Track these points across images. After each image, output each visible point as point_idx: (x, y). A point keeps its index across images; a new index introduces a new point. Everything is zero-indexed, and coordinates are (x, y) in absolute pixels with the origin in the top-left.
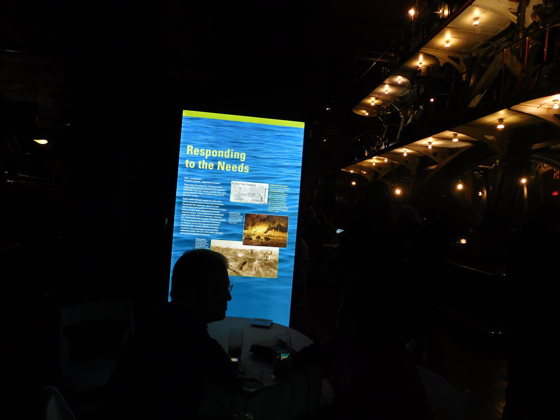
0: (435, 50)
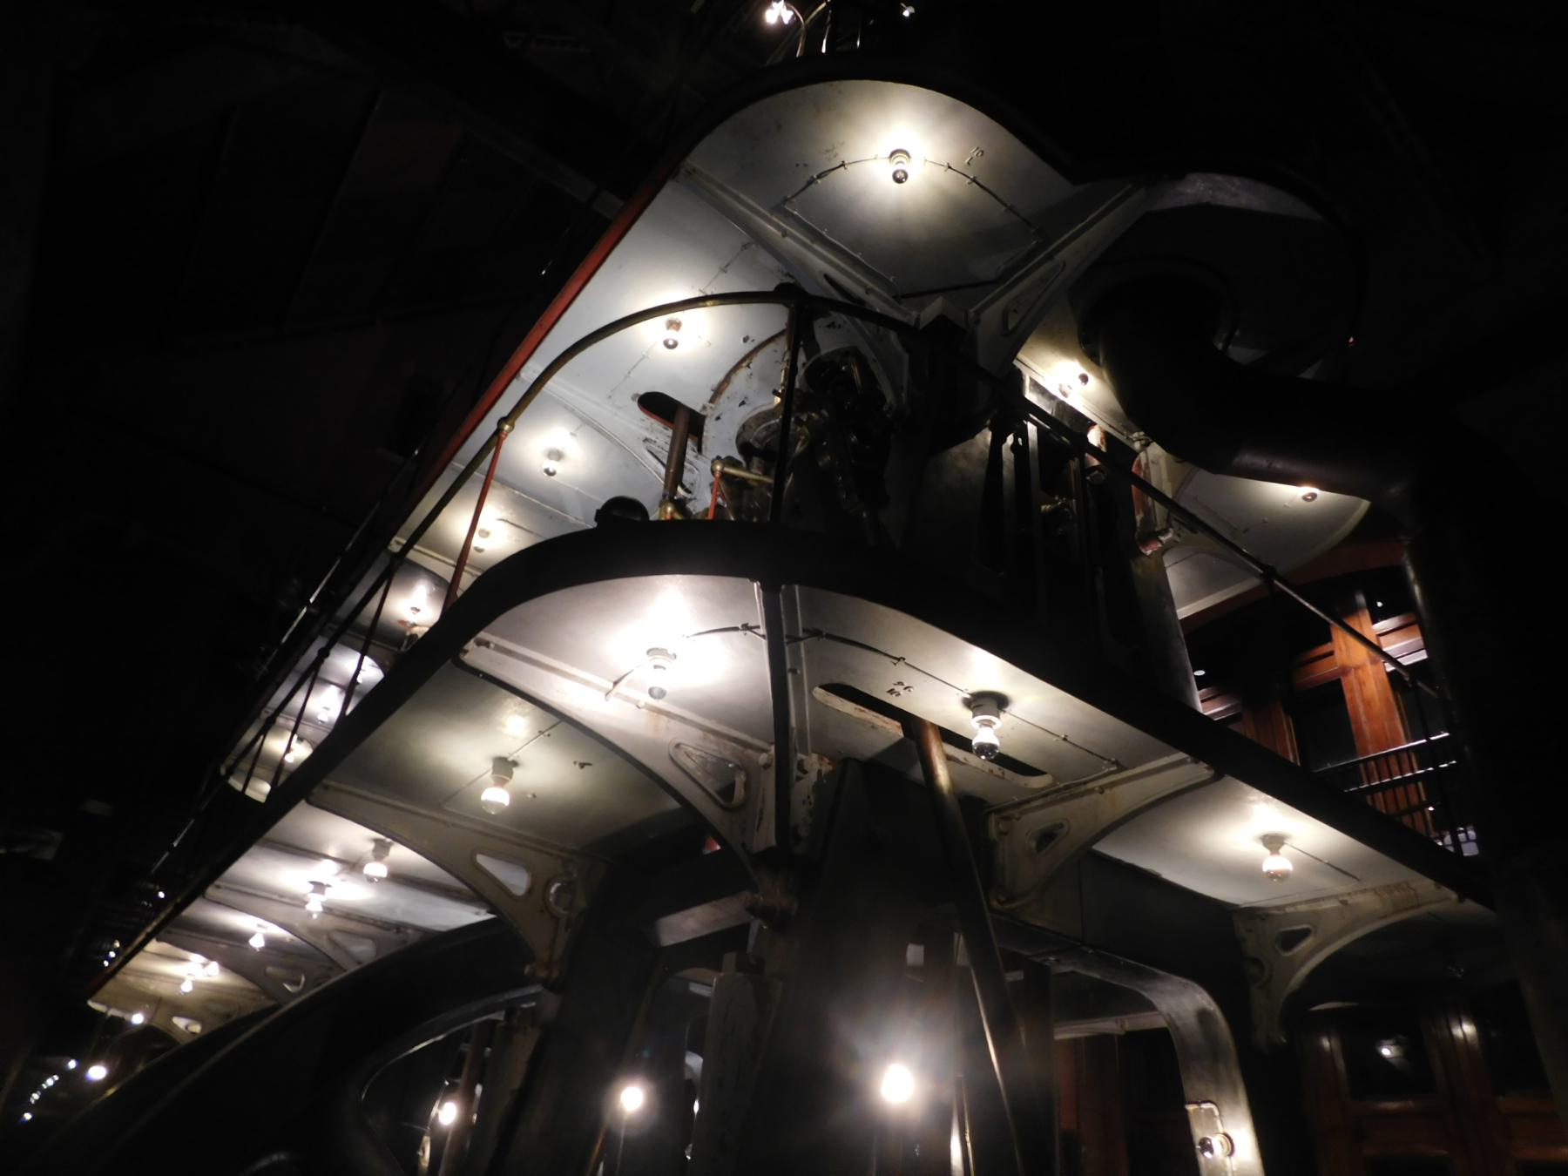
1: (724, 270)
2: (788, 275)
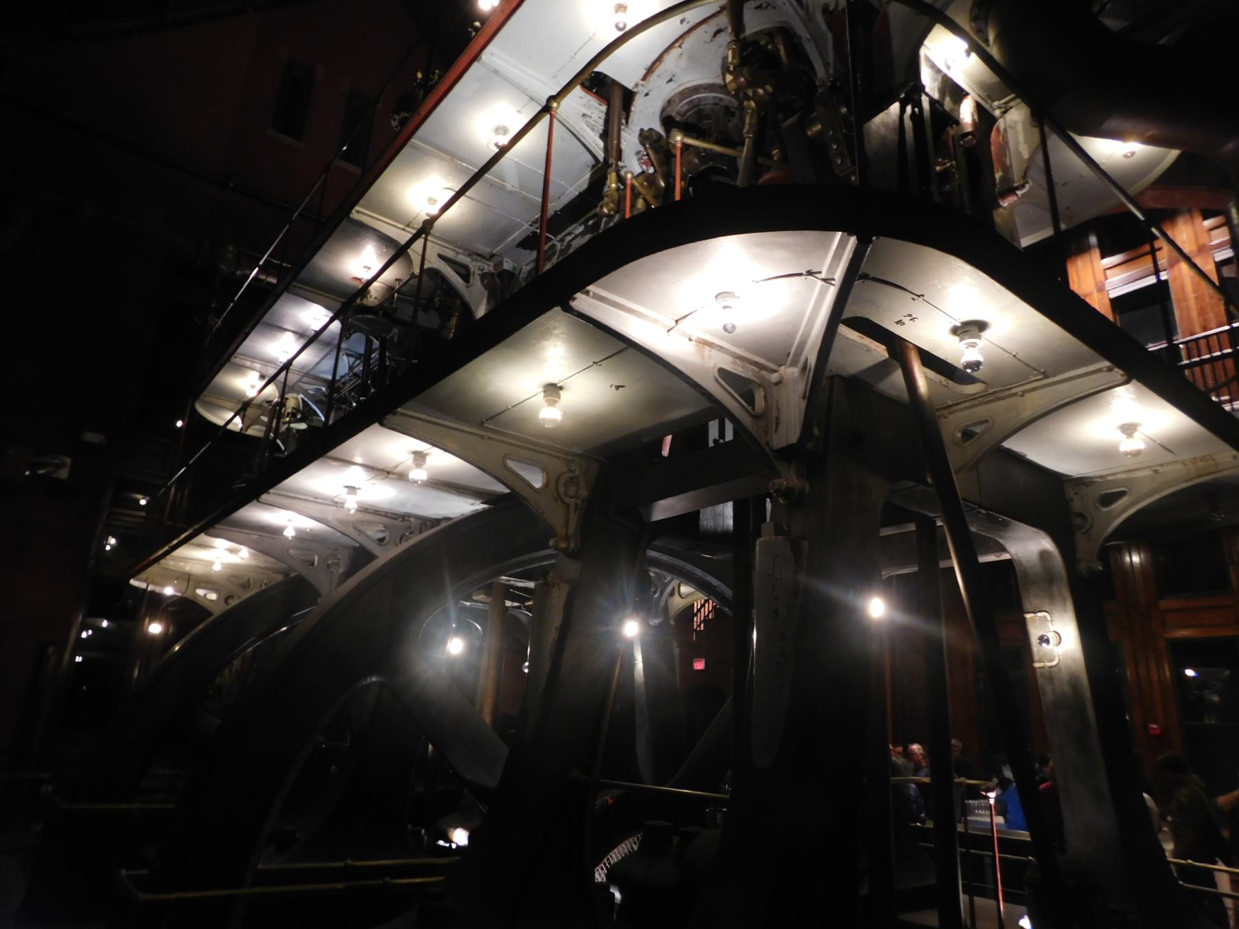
0: (403, 227)
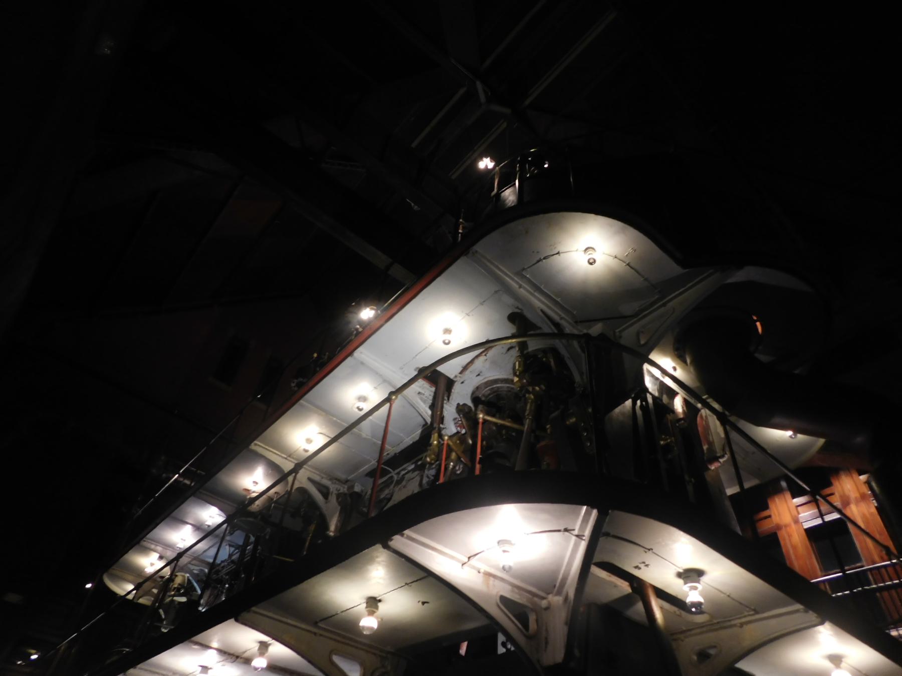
0: (286, 456)
1: (482, 304)
2: (517, 308)
